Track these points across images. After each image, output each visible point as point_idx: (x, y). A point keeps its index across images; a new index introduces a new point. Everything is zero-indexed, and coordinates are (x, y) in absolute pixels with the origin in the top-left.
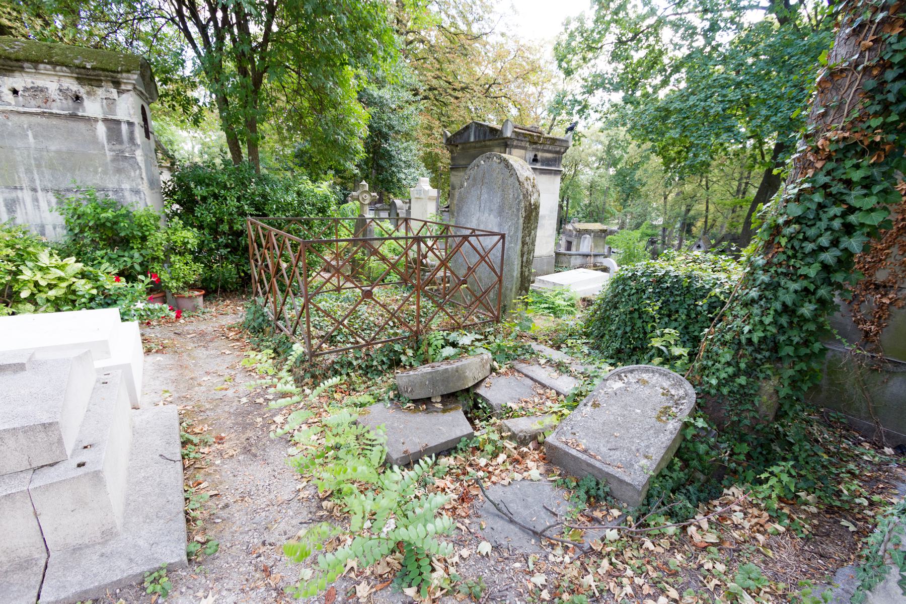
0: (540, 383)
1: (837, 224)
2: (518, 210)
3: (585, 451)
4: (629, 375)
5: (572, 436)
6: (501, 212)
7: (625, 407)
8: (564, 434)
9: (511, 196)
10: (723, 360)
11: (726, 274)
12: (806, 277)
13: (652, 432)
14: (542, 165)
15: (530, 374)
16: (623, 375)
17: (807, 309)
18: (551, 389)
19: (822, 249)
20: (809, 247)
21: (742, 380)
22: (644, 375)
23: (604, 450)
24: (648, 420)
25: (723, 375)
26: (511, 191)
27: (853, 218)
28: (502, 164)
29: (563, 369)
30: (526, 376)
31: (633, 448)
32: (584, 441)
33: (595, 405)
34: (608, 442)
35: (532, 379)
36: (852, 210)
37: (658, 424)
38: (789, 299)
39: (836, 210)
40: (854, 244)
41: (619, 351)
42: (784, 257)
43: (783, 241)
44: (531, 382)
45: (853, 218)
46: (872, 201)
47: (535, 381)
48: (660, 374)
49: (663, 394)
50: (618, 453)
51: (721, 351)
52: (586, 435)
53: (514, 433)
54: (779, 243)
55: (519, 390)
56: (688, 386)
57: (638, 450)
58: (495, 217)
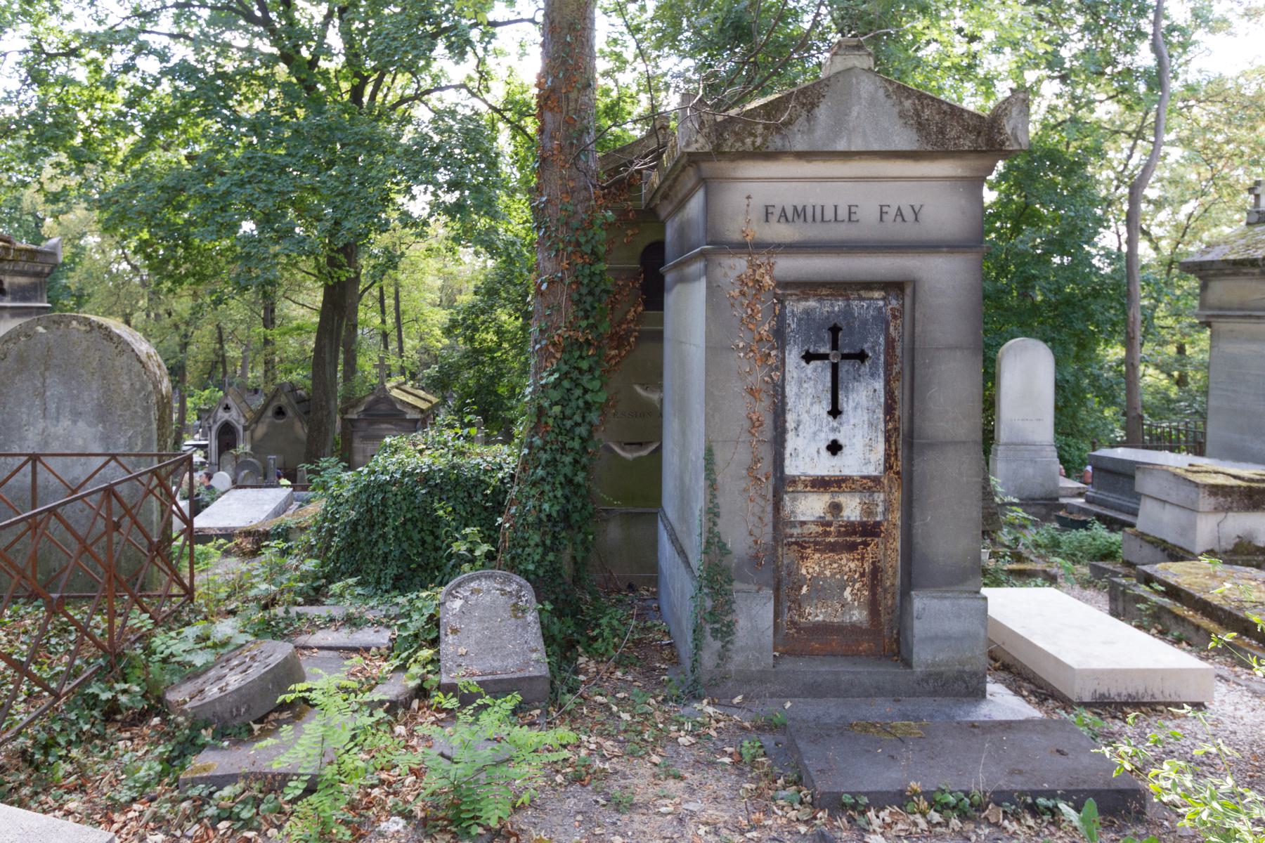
1: (581, 403)
2: (147, 409)
6: (103, 414)
9: (126, 386)
10: (532, 543)
11: (498, 458)
12: (572, 449)
14: (14, 300)
15: (323, 643)
17: (580, 478)
19: (577, 424)
20: (569, 423)
21: (551, 557)
25: (537, 557)
26: (124, 378)
27: (588, 397)
28: (96, 334)
30: (321, 648)
33: (455, 631)
35: (330, 648)
36: (586, 391)
37: (519, 621)
38: (568, 470)
39: (578, 392)
40: (594, 417)
41: (397, 578)
42: (553, 435)
43: (550, 421)
45: (588, 397)
46: (597, 384)
51: (527, 535)
53: (391, 702)
54: (546, 423)
58: (90, 425)
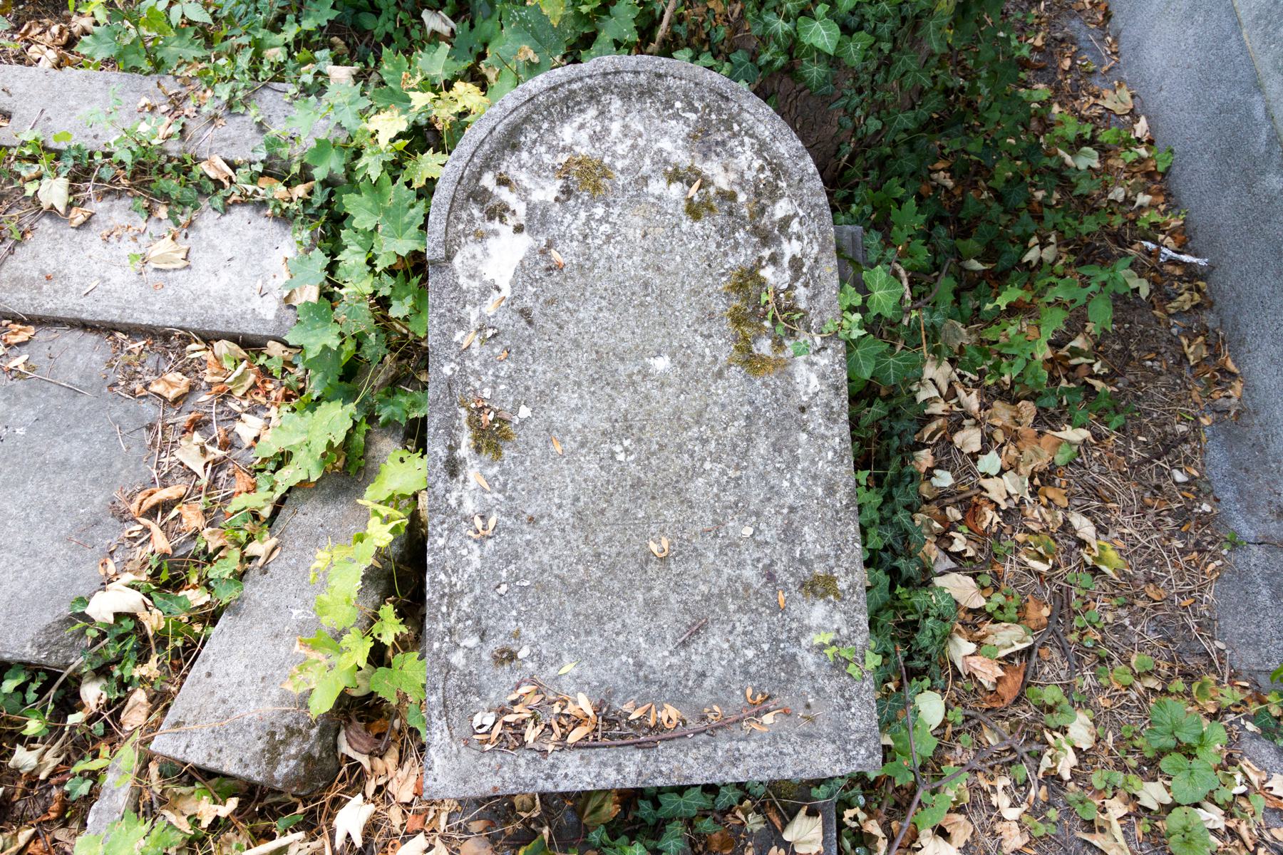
0: (134, 331)
3: (611, 728)
4: (509, 165)
5: (505, 675)
7: (601, 375)
8: (471, 687)
13: (763, 446)
16: (488, 180)
18: (208, 339)
22: (567, 133)
23: (659, 657)
24: (718, 388)
29: (172, 185)
31: (749, 573)
32: (569, 668)
34: (652, 608)
44: (86, 355)
47: (106, 329)
48: (625, 95)
49: (694, 211)
50: (716, 639)
52: (557, 629)
55: (75, 451)
56: (761, 119)
57: (771, 577)
